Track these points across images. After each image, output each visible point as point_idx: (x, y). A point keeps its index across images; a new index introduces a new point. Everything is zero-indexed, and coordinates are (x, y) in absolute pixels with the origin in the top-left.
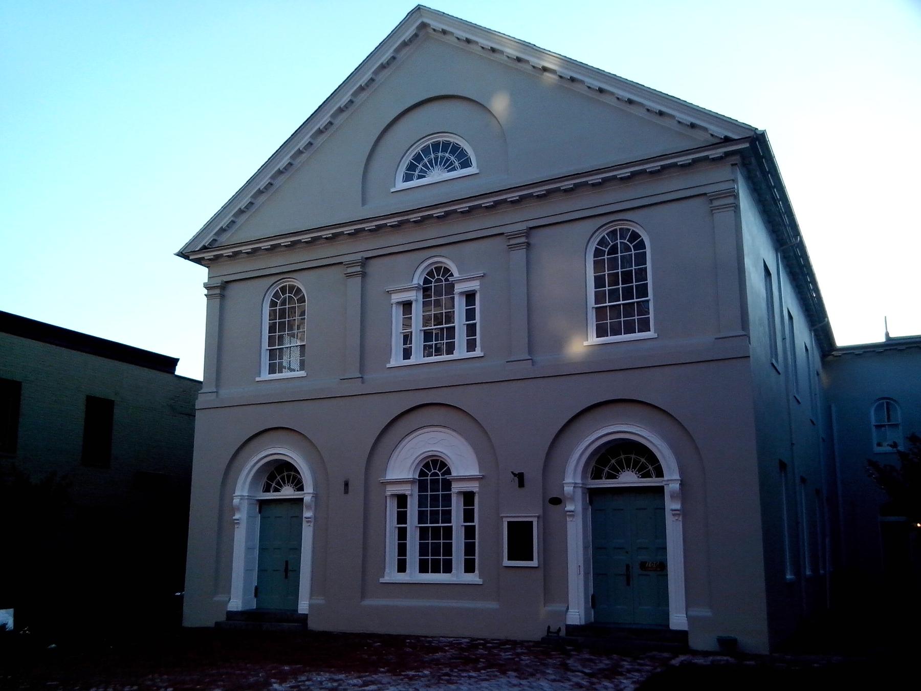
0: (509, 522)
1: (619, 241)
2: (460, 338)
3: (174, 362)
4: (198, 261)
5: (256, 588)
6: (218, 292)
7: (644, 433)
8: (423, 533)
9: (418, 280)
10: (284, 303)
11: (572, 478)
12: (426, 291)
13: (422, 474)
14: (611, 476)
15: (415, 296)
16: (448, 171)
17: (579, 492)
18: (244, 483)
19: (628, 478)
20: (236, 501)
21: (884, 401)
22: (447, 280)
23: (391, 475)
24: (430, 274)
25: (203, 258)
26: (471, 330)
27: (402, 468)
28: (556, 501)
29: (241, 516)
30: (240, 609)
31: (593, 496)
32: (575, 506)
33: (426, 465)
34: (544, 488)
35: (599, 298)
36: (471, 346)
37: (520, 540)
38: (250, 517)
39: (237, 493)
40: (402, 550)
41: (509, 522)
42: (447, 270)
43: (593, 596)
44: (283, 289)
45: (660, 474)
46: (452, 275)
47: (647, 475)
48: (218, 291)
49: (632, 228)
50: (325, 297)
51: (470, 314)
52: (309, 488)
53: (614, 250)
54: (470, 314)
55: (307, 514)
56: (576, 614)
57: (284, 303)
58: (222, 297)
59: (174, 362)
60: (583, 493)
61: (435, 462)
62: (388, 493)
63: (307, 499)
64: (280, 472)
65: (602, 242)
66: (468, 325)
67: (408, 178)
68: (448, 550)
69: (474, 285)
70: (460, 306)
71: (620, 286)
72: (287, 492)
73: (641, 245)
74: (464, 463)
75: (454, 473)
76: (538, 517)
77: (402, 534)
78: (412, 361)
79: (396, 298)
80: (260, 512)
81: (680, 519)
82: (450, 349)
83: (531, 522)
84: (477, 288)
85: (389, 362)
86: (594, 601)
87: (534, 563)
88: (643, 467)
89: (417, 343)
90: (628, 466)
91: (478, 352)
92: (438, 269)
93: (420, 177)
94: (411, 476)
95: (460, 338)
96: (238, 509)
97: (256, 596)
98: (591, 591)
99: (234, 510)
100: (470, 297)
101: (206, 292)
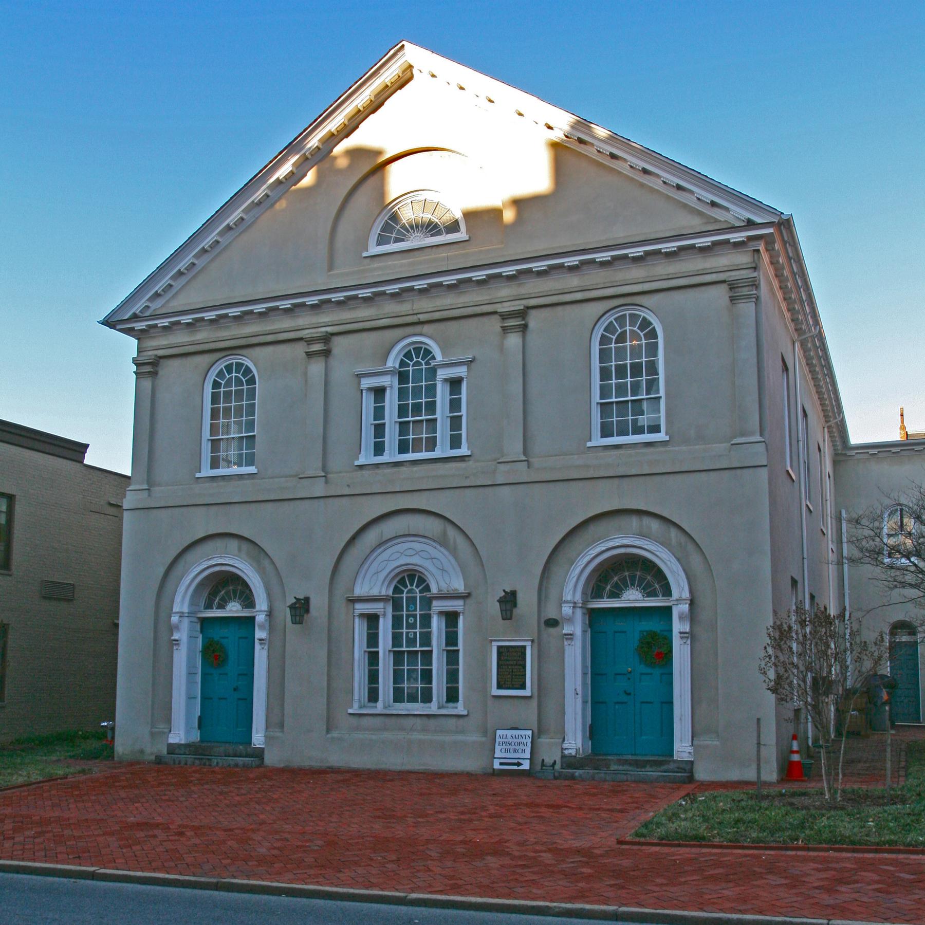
0: (499, 648)
1: (628, 328)
2: (443, 431)
3: (82, 448)
4: (129, 332)
5: (200, 718)
6: (148, 368)
7: (182, 589)
8: (398, 657)
9: (393, 362)
10: (229, 383)
11: (181, 603)
12: (403, 377)
13: (397, 590)
14: (615, 595)
15: (390, 382)
16: (432, 235)
17: (579, 612)
18: (184, 597)
19: (632, 598)
20: (175, 619)
21: (405, 575)
22: (427, 363)
23: (360, 590)
24: (408, 355)
25: (132, 329)
26: (455, 423)
27: (373, 583)
28: (552, 623)
29: (182, 635)
30: (183, 742)
31: (594, 617)
32: (576, 627)
33: (402, 582)
34: (539, 611)
35: (605, 392)
36: (455, 442)
37: (511, 667)
38: (191, 637)
39: (176, 609)
40: (373, 677)
41: (499, 648)
42: (428, 352)
43: (591, 727)
44: (229, 368)
45: (667, 592)
46: (433, 358)
47: (652, 594)
48: (148, 369)
49: (643, 314)
50: (274, 374)
51: (455, 405)
52: (262, 604)
53: (621, 338)
54: (455, 405)
55: (259, 634)
56: (575, 742)
57: (229, 383)
58: (154, 374)
59: (82, 448)
60: (584, 614)
61: (412, 577)
62: (357, 612)
63: (260, 618)
64: (224, 585)
65: (609, 328)
66: (452, 418)
67: (381, 241)
68: (427, 676)
69: (461, 371)
70: (442, 395)
71: (629, 379)
72: (234, 609)
73: (653, 334)
74: (446, 577)
75: (434, 589)
76: (532, 641)
77: (373, 658)
78: (385, 458)
79: (366, 383)
80: (202, 632)
81: (689, 642)
82: (431, 444)
83: (524, 647)
84: (464, 374)
85: (358, 459)
86: (593, 732)
87: (527, 692)
88: (649, 585)
89: (391, 437)
90: (639, 585)
91: (464, 451)
92: (417, 350)
93: (397, 240)
94: (384, 593)
95: (443, 431)
96: (177, 628)
97: (200, 727)
98: (589, 721)
99: (172, 629)
100: (455, 384)
101: (134, 368)
